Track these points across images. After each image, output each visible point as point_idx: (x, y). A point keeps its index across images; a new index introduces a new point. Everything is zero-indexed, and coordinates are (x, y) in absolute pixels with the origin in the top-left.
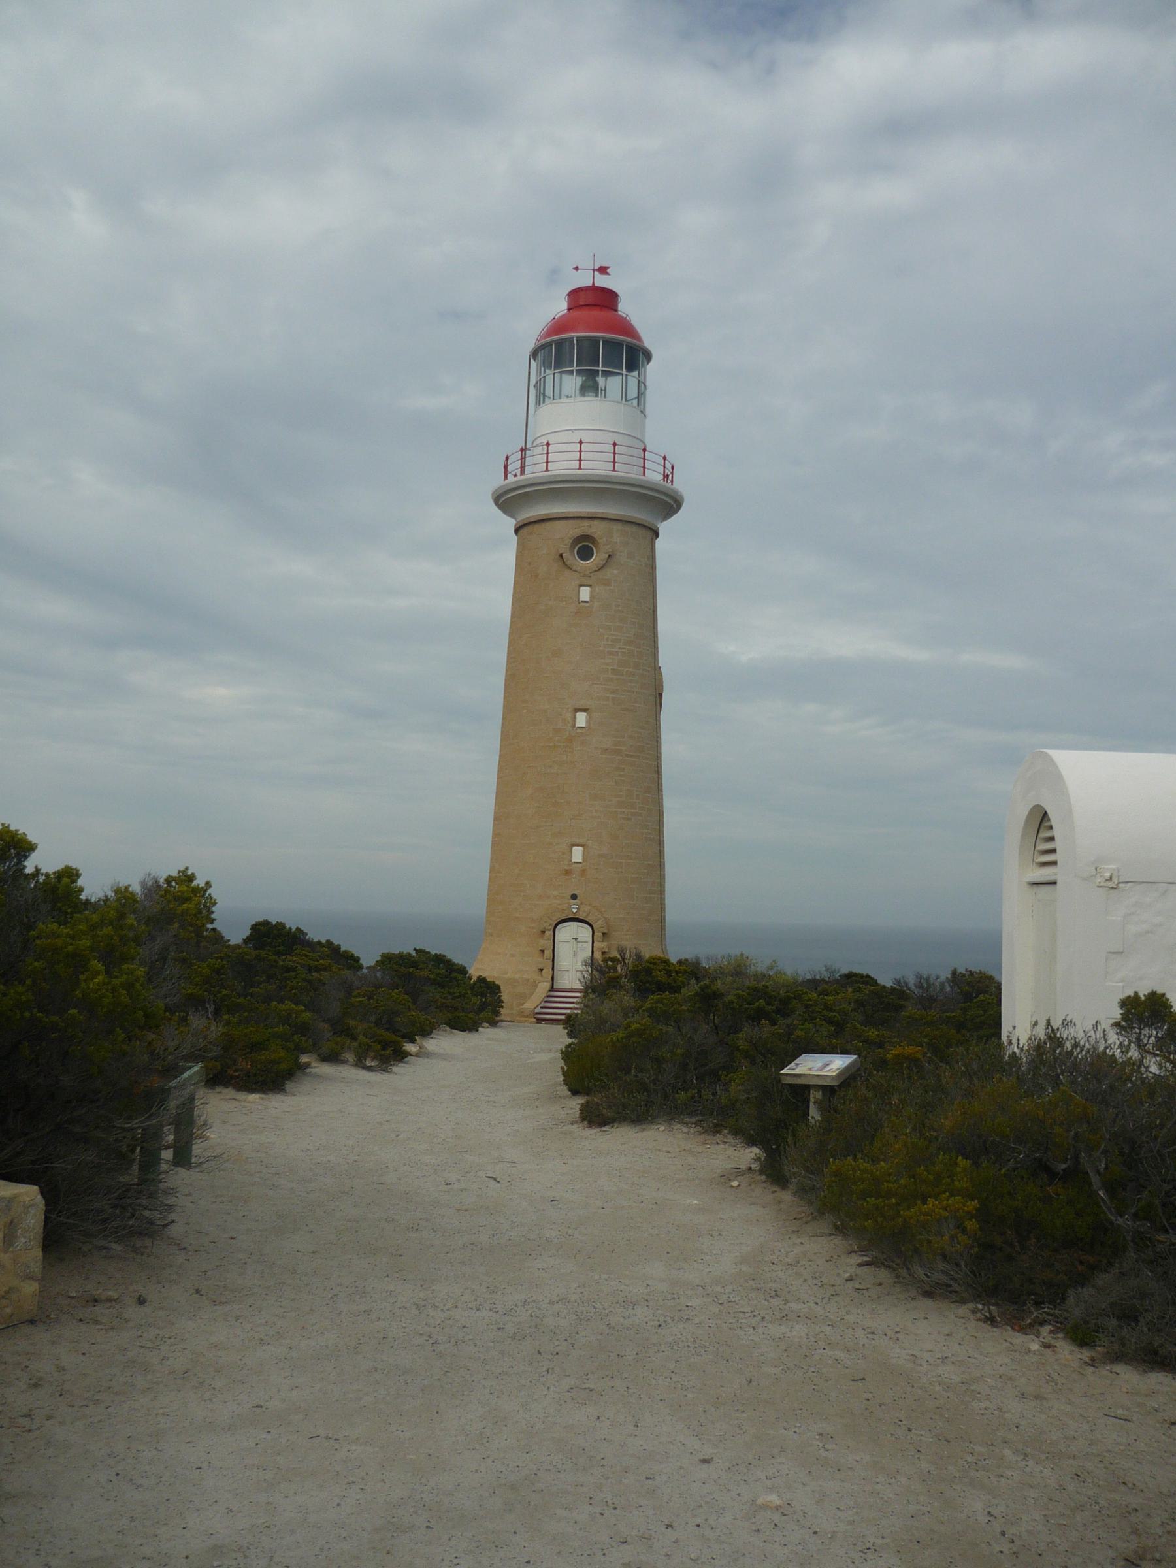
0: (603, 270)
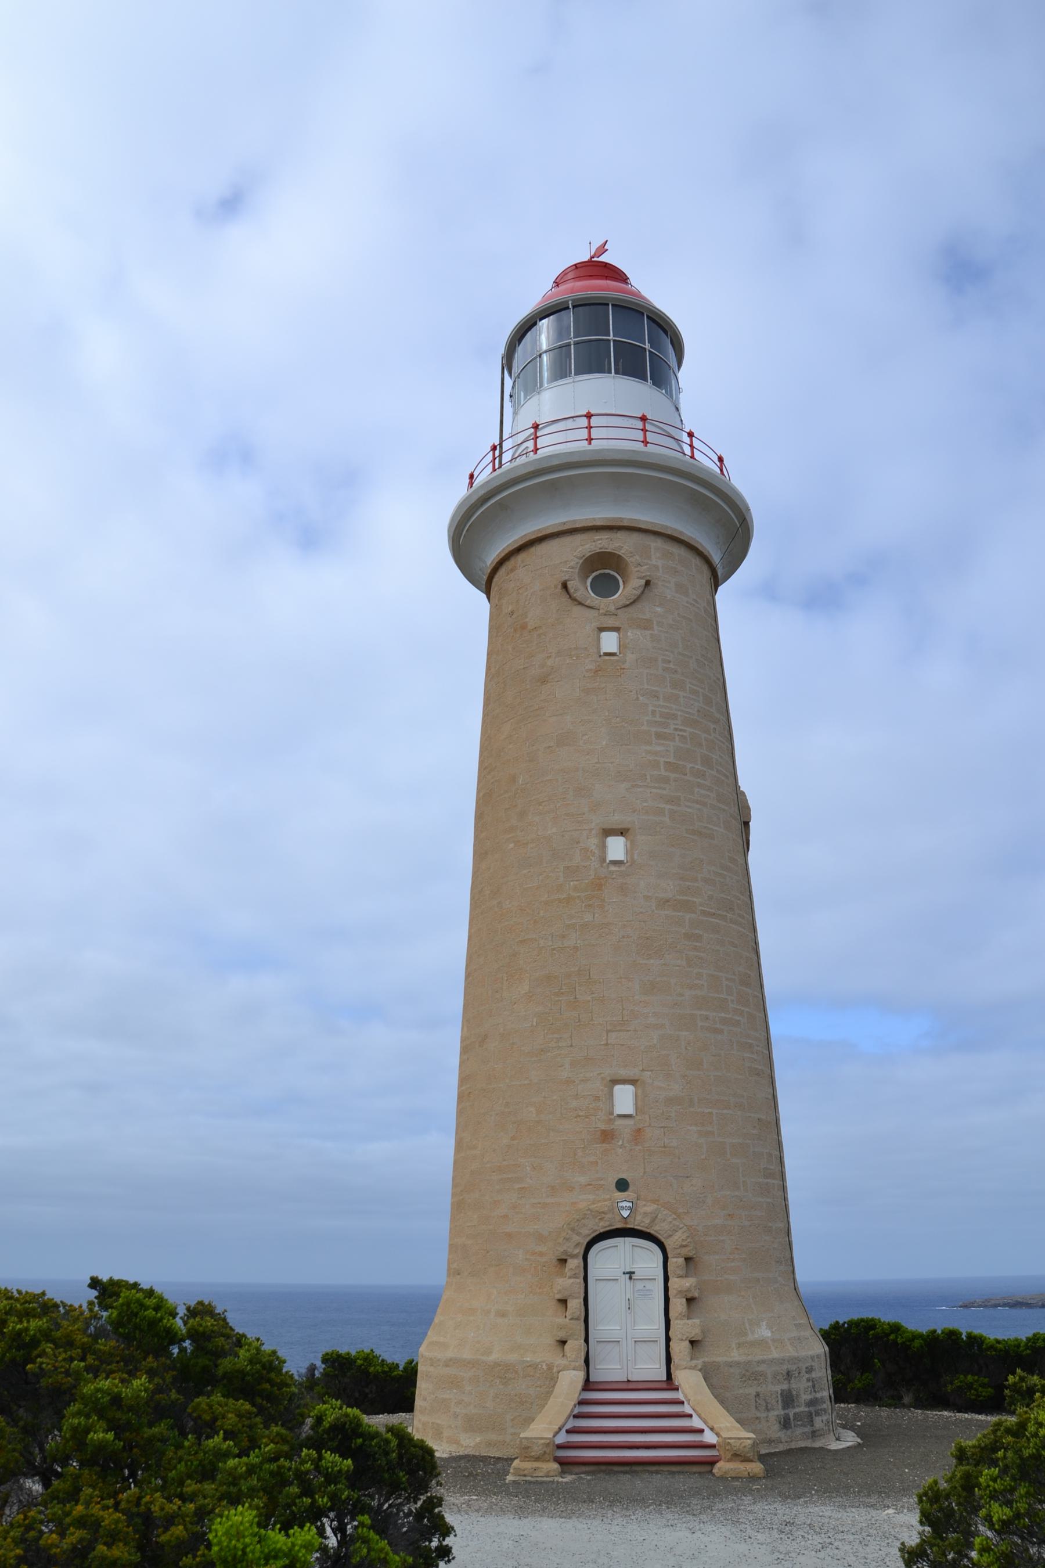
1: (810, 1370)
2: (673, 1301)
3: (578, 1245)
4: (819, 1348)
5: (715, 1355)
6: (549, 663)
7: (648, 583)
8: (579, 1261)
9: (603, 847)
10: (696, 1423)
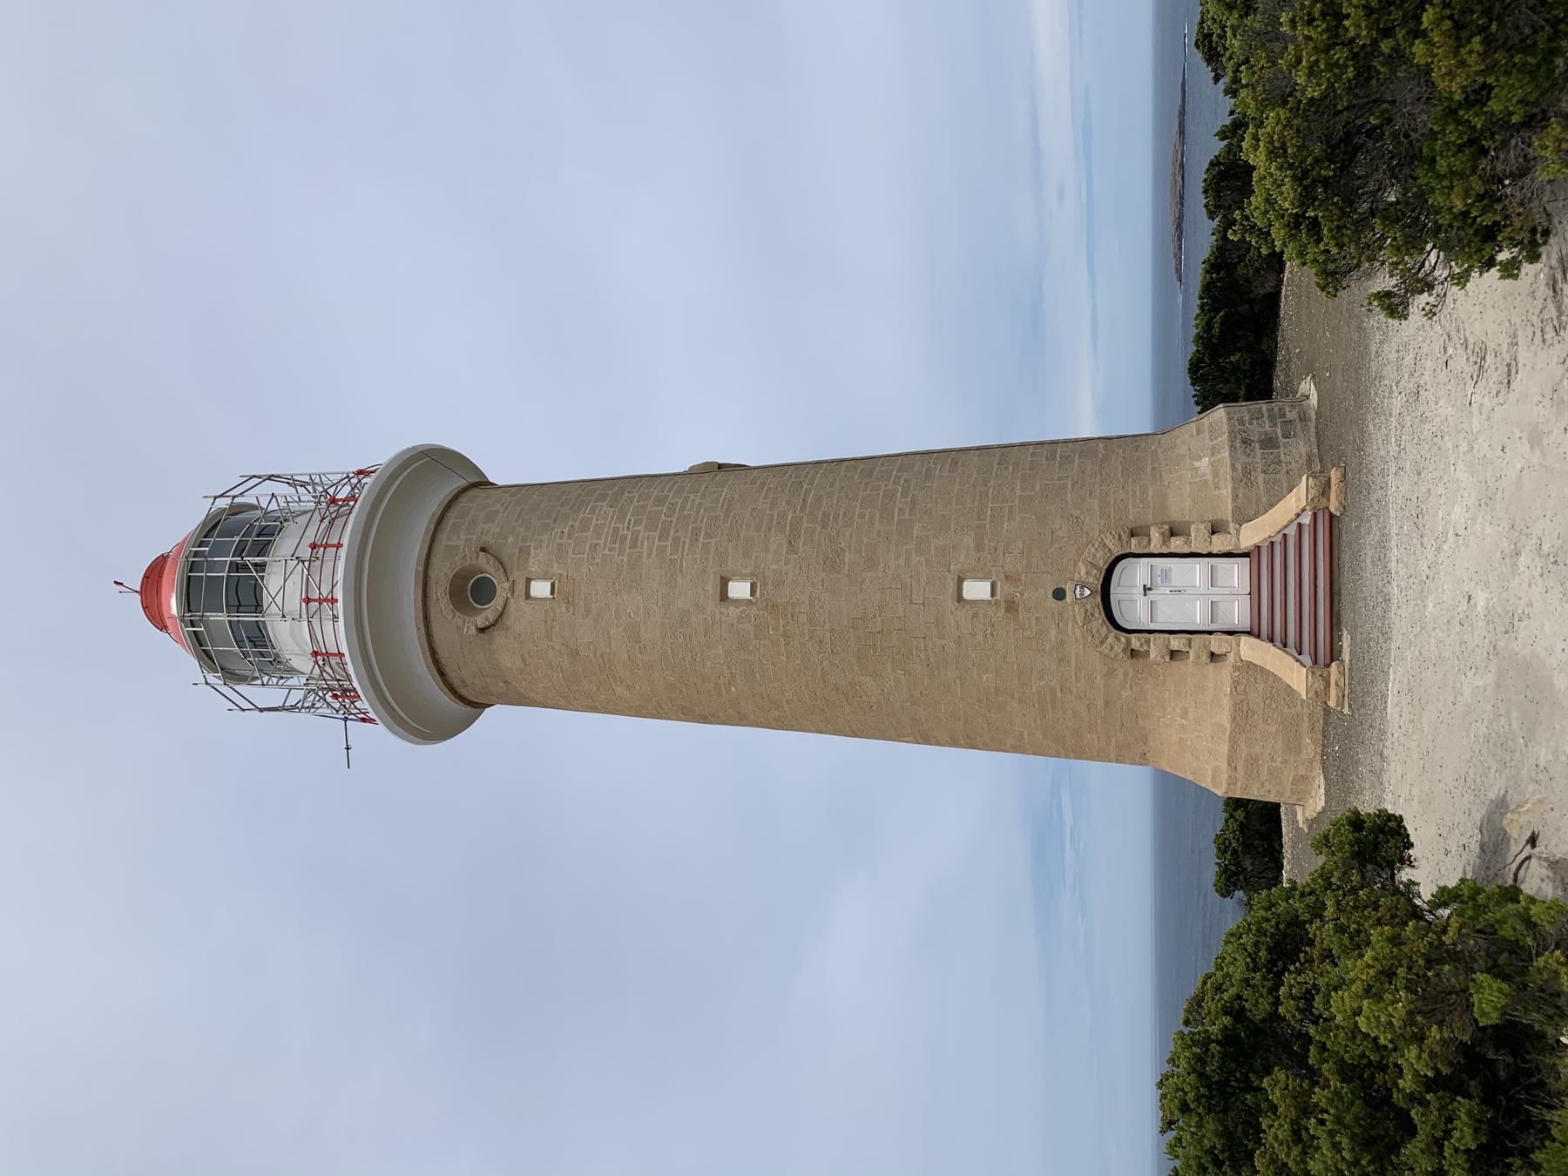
1: (1242, 422)
2: (1172, 550)
3: (1117, 638)
4: (1219, 413)
5: (1226, 512)
6: (557, 647)
7: (483, 550)
8: (1134, 638)
9: (737, 602)
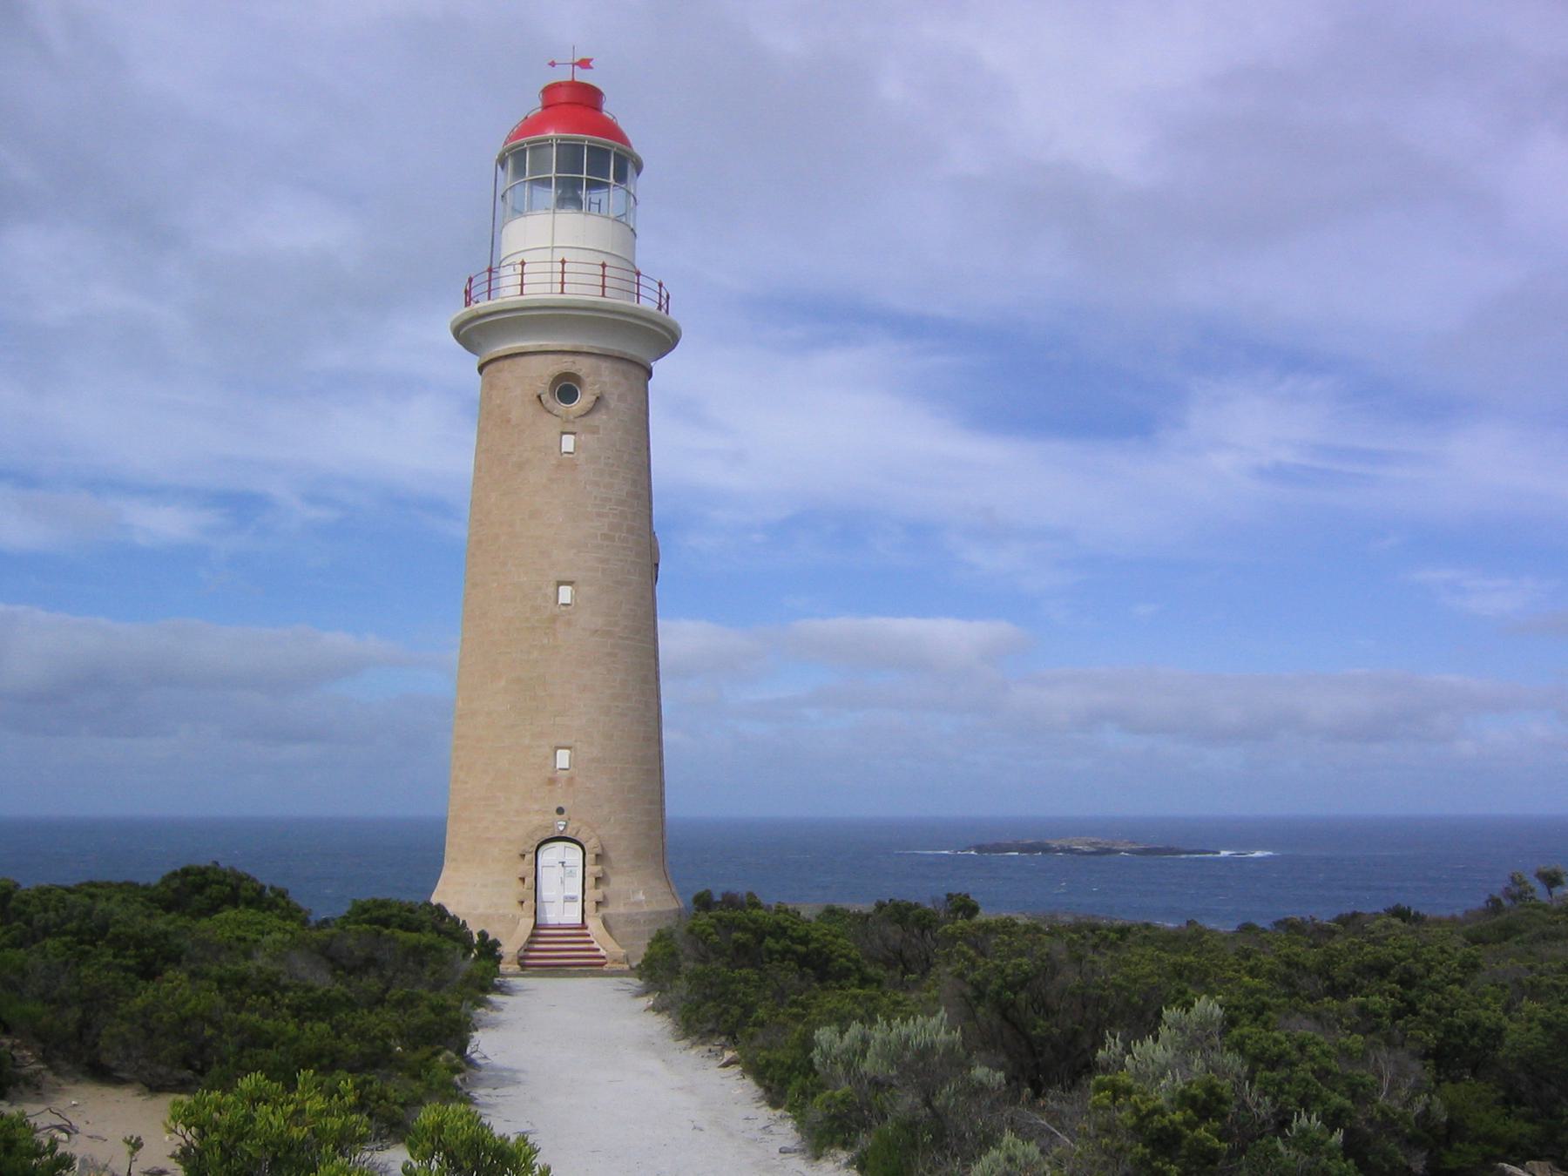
0: (585, 64)
10: (596, 945)
